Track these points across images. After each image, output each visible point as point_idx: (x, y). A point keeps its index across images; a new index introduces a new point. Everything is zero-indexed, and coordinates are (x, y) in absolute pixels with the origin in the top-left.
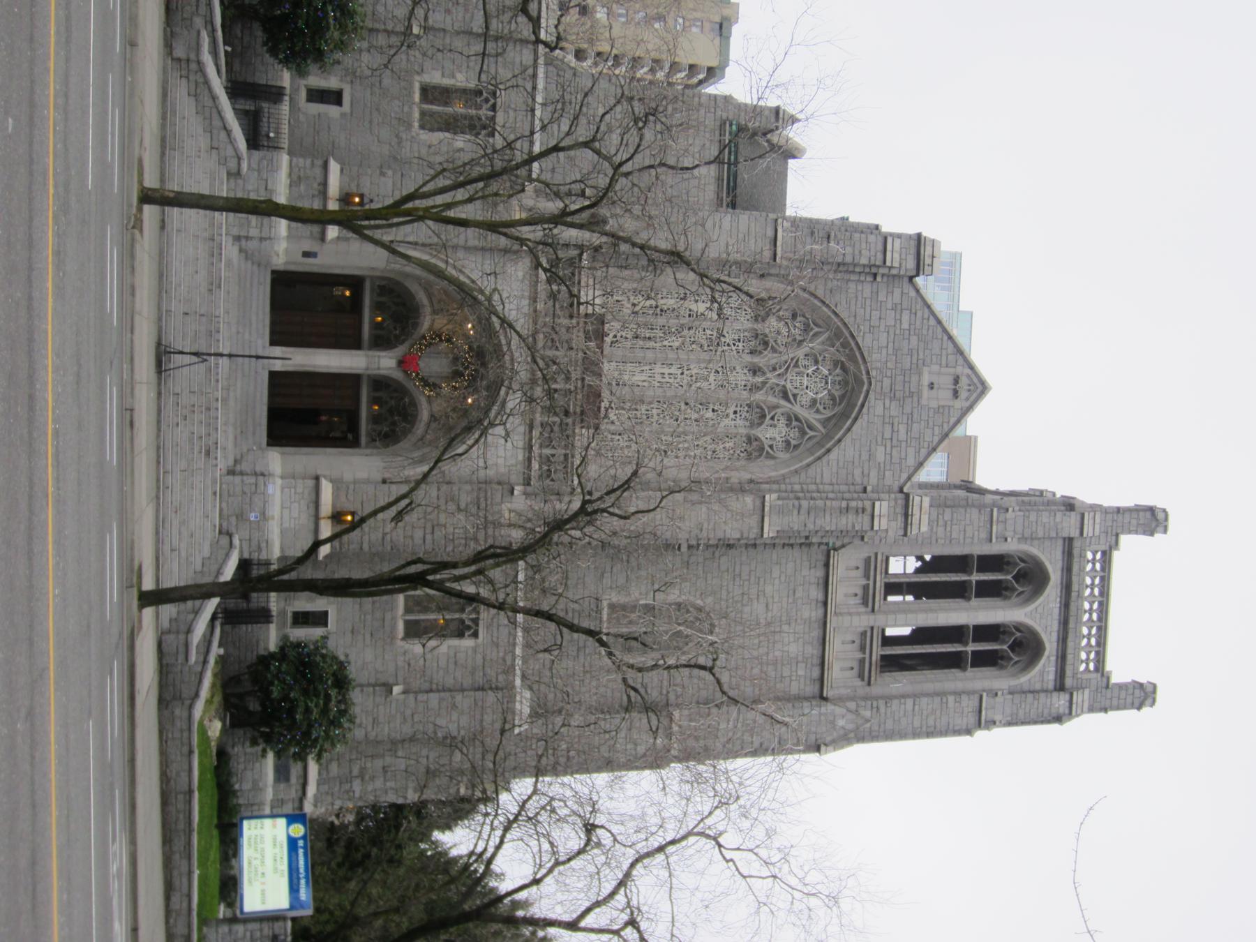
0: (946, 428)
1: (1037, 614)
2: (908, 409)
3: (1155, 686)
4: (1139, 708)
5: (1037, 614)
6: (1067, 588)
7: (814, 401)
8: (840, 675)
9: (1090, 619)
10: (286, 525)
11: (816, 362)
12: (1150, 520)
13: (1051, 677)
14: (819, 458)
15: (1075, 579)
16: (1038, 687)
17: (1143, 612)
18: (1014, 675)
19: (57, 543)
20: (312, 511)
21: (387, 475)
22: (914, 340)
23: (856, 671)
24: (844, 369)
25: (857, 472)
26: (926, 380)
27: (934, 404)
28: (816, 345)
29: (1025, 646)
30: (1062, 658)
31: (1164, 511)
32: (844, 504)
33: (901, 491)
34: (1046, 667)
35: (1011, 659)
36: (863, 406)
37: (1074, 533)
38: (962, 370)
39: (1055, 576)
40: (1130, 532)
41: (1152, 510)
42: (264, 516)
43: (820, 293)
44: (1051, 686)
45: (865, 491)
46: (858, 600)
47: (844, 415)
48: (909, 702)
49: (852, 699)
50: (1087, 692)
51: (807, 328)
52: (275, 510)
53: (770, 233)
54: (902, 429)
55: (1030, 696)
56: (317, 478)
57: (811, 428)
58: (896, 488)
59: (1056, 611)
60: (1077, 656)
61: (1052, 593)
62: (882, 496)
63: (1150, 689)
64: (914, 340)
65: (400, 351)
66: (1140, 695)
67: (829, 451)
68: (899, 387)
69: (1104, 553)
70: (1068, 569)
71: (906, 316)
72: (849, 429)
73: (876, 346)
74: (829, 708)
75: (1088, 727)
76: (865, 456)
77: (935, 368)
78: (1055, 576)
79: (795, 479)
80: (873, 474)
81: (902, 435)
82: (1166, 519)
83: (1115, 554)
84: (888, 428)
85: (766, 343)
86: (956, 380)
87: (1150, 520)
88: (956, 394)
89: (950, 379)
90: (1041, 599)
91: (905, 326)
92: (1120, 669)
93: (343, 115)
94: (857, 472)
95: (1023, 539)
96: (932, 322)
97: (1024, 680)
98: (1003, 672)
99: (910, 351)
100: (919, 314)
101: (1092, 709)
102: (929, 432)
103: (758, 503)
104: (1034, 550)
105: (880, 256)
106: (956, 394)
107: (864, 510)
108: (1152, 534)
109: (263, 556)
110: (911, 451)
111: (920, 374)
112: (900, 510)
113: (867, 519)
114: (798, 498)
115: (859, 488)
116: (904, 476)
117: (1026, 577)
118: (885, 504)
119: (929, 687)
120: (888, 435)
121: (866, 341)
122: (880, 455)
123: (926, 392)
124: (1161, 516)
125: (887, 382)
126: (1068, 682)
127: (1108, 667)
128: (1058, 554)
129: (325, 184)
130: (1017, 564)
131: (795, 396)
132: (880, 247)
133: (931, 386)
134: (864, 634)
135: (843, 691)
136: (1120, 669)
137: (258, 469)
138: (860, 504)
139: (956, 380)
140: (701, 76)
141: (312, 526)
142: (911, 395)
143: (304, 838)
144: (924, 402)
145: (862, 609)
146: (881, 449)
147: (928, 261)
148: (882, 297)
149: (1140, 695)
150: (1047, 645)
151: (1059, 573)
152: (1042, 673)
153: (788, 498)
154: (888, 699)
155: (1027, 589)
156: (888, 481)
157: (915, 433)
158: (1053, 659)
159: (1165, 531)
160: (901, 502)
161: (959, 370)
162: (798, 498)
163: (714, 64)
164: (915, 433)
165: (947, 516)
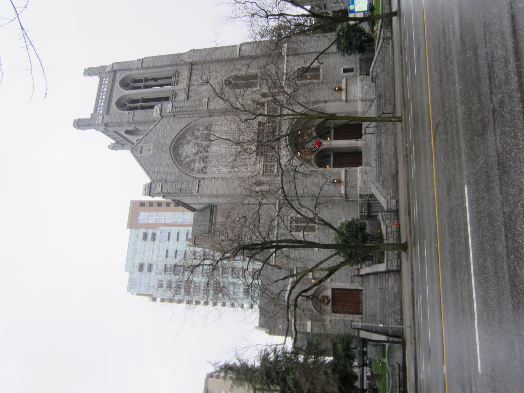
0: (146, 137)
1: (120, 92)
2: (158, 142)
3: (84, 74)
4: (90, 68)
5: (120, 92)
6: (110, 101)
7: (188, 143)
8: (185, 74)
9: (103, 93)
10: (356, 86)
11: (187, 156)
12: (80, 124)
13: (118, 75)
14: (188, 125)
15: (111, 83)
16: (123, 72)
17: (85, 94)
18: (130, 75)
19: (429, 106)
20: (348, 91)
21: (325, 104)
22: (154, 163)
23: (180, 74)
24: (178, 154)
25: (176, 122)
26: (151, 151)
27: (149, 144)
28: (187, 160)
29: (125, 84)
30: (114, 80)
32: (181, 109)
33: (162, 117)
34: (119, 77)
36: (173, 142)
37: (105, 116)
38: (139, 155)
39: (113, 104)
40: (87, 119)
42: (362, 88)
43: (184, 175)
44: (118, 72)
45: (174, 116)
46: (178, 95)
47: (179, 139)
48: (164, 64)
49: (182, 65)
50: (107, 71)
51: (189, 166)
52: (359, 89)
53: (200, 189)
54: (160, 136)
55: (125, 68)
56: (347, 101)
57: (190, 135)
58: (164, 118)
59: (114, 94)
60: (108, 83)
61: (115, 98)
62: (168, 114)
63: (86, 74)
64: (154, 163)
65: (322, 148)
66: (89, 72)
67: (185, 127)
68: (160, 148)
69: (96, 112)
70: (109, 106)
71: (156, 170)
72: (178, 134)
73: (167, 157)
74: (189, 61)
75: (107, 60)
76: (173, 127)
77: (148, 155)
78: (113, 104)
79: (196, 118)
80: (171, 122)
81: (160, 134)
82: (74, 123)
83: (92, 112)
84: (165, 136)
85: (203, 160)
86: (141, 152)
87: (80, 124)
88: (142, 148)
89: (143, 152)
90: (121, 78)
91: (157, 168)
92: (96, 80)
93: (341, 219)
94: (176, 122)
95: (123, 114)
96: (147, 169)
97: (127, 73)
98: (133, 77)
99: (156, 159)
100: (152, 171)
101: (106, 67)
102: (152, 136)
103: (209, 107)
104: (120, 111)
105: (164, 185)
106: (142, 148)
107: (175, 108)
108: (79, 119)
109: (362, 77)
110: (158, 129)
111: (153, 153)
112: (163, 110)
113: (174, 105)
114: (196, 111)
115: (176, 117)
116: (161, 122)
117: (121, 105)
118: (168, 111)
119: (158, 70)
120: (165, 134)
121: (170, 161)
122: (168, 127)
123: (151, 148)
124: (76, 125)
125: (164, 149)
126: (112, 74)
127: (99, 79)
128: (111, 111)
129: (346, 186)
131: (195, 145)
132: (163, 189)
133: (149, 150)
134: (177, 85)
135: (183, 67)
136: (96, 80)
137: (365, 102)
138: (176, 110)
139: (141, 152)
140: (215, 374)
141: (348, 86)
142: (156, 146)
143: (349, 5)
144: (152, 145)
145: (177, 92)
146: (168, 129)
147: (147, 188)
148: (164, 176)
149: (89, 72)
151: (112, 105)
152: (121, 75)
153: (199, 110)
154: (171, 65)
155: (123, 101)
156: (166, 120)
157: (156, 135)
158: (117, 80)
159: (75, 120)
160: (163, 113)
161: (140, 155)
162: (196, 111)
163: (210, 379)
164: (156, 135)
165: (147, 118)
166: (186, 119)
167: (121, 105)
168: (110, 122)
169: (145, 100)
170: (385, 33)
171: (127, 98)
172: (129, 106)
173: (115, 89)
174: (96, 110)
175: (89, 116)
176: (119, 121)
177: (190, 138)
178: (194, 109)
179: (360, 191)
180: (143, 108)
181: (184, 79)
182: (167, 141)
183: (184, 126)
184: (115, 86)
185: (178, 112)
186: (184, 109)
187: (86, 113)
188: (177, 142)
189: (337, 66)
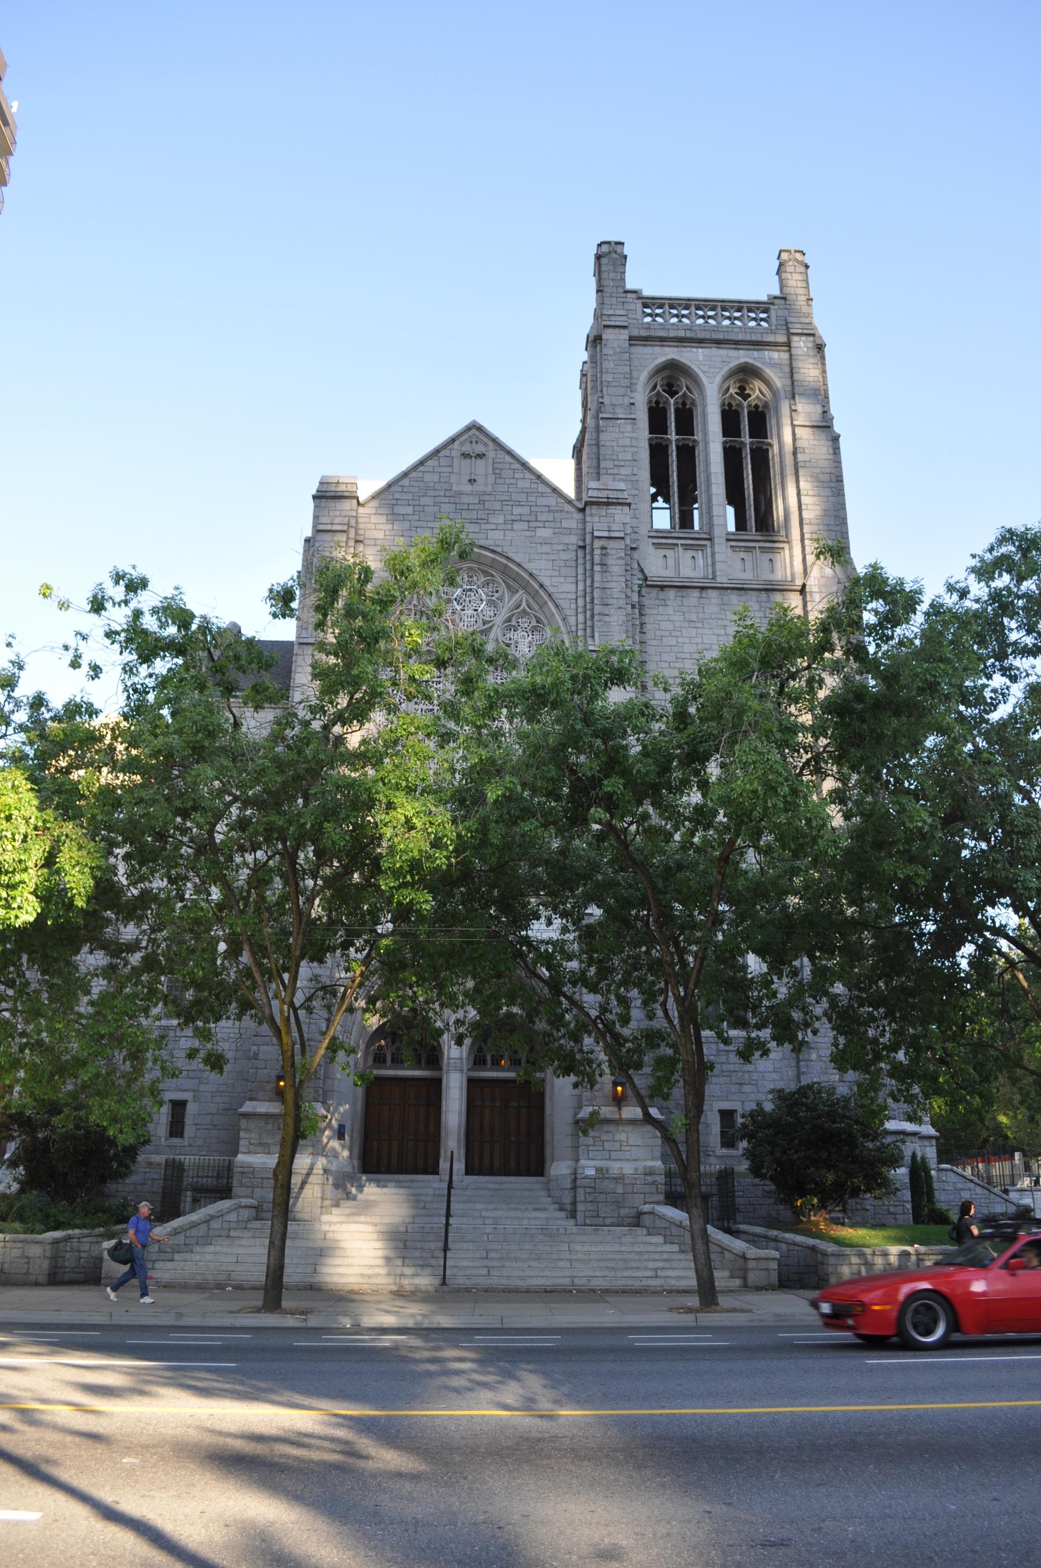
2: (498, 506)
5: (711, 372)
6: (681, 341)
12: (610, 259)
22: (424, 501)
25: (564, 556)
26: (467, 488)
27: (491, 479)
31: (599, 245)
35: (684, 395)
37: (624, 335)
41: (598, 258)
47: (505, 571)
54: (517, 511)
58: (580, 516)
59: (707, 351)
61: (693, 358)
64: (424, 501)
67: (541, 586)
68: (474, 515)
72: (519, 565)
76: (546, 548)
77: (454, 478)
79: (572, 620)
81: (525, 510)
86: (465, 456)
87: (610, 259)
88: (481, 456)
91: (409, 510)
96: (405, 482)
104: (644, 376)
106: (481, 456)
109: (661, 1179)
111: (460, 494)
115: (580, 553)
117: (672, 376)
120: (525, 526)
123: (478, 487)
124: (605, 248)
130: (658, 393)
133: (472, 481)
136: (761, 287)
139: (465, 456)
150: (742, 360)
151: (666, 349)
155: (684, 381)
156: (573, 524)
157: (522, 498)
159: (622, 244)
160: (594, 510)
166: (573, 588)
167: (672, 376)
168: (605, 351)
169: (688, 455)
170: (763, 1265)
171: (695, 396)
172: (667, 402)
173: (723, 352)
174: (649, 302)
175: (631, 282)
176: (608, 377)
177: (508, 603)
178: (597, 609)
179: (657, 1159)
180: (658, 453)
181: (755, 568)
182: (499, 535)
183: (546, 582)
184: (733, 353)
185: (592, 560)
186: (597, 577)
187: (643, 277)
188: (493, 564)
189: (747, 1088)
